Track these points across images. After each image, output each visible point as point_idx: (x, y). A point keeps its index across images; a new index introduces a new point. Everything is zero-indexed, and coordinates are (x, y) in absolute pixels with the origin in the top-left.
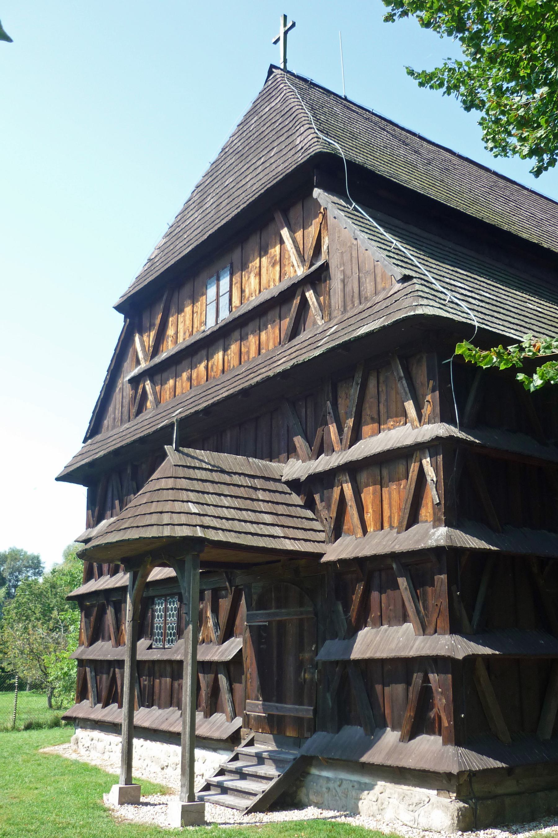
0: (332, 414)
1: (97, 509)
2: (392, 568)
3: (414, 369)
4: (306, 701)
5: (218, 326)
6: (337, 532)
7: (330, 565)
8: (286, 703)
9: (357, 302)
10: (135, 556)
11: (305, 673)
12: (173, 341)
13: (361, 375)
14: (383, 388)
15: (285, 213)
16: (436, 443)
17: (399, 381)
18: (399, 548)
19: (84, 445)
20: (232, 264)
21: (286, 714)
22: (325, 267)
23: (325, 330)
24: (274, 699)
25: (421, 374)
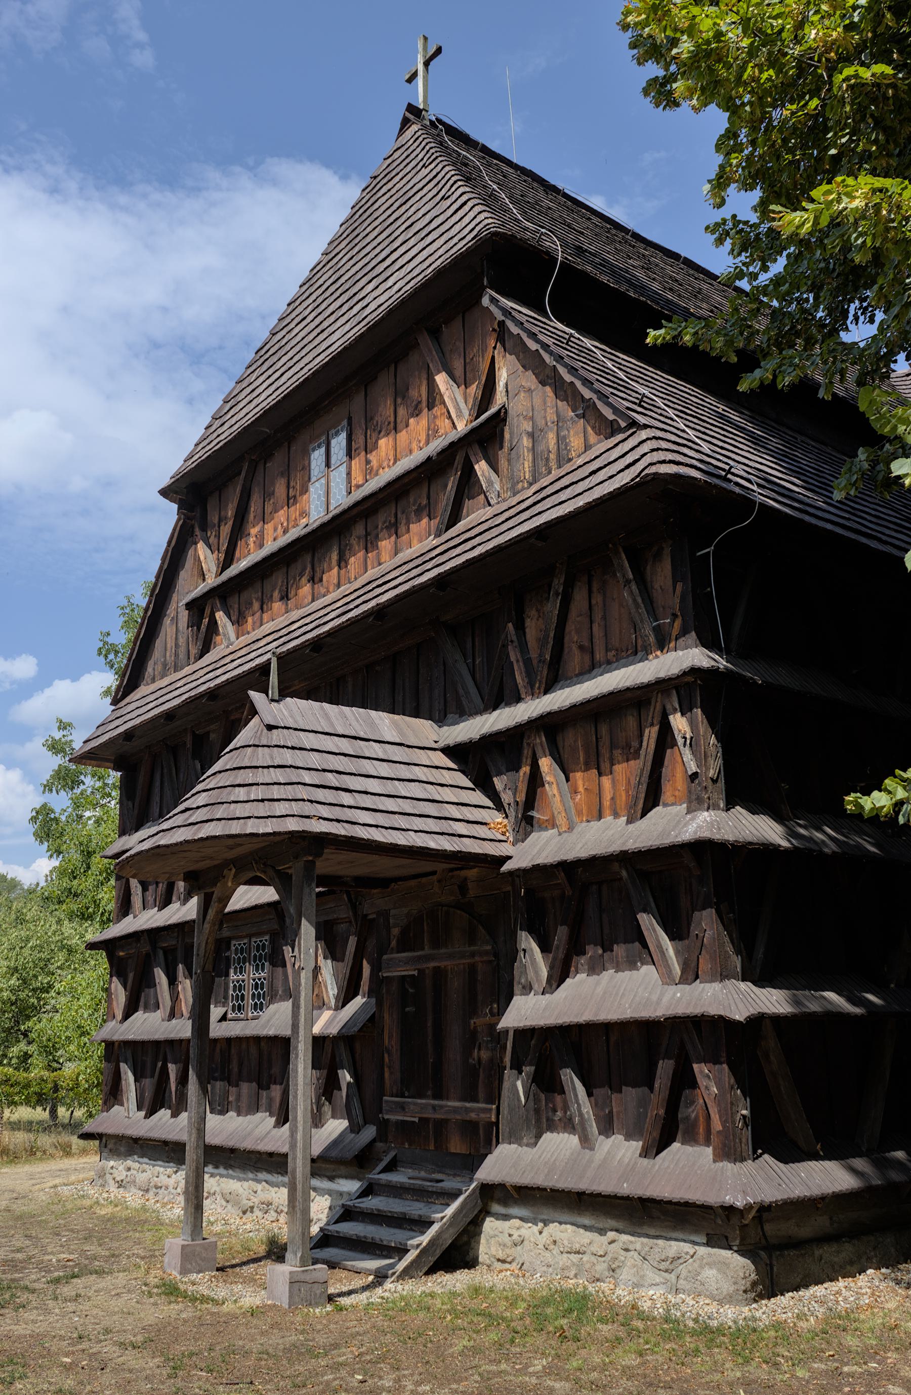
0: (516, 644)
1: (138, 810)
2: (621, 879)
3: (648, 568)
4: (481, 1095)
5: (330, 515)
6: (526, 822)
7: (518, 876)
8: (448, 1099)
9: (553, 464)
10: (207, 868)
11: (479, 1049)
12: (258, 543)
13: (562, 581)
14: (597, 599)
15: (435, 334)
16: (690, 679)
17: (625, 586)
18: (632, 845)
19: (113, 707)
20: (350, 420)
21: (449, 1117)
22: (500, 418)
23: (504, 509)
24: (429, 1093)
25: (662, 575)
